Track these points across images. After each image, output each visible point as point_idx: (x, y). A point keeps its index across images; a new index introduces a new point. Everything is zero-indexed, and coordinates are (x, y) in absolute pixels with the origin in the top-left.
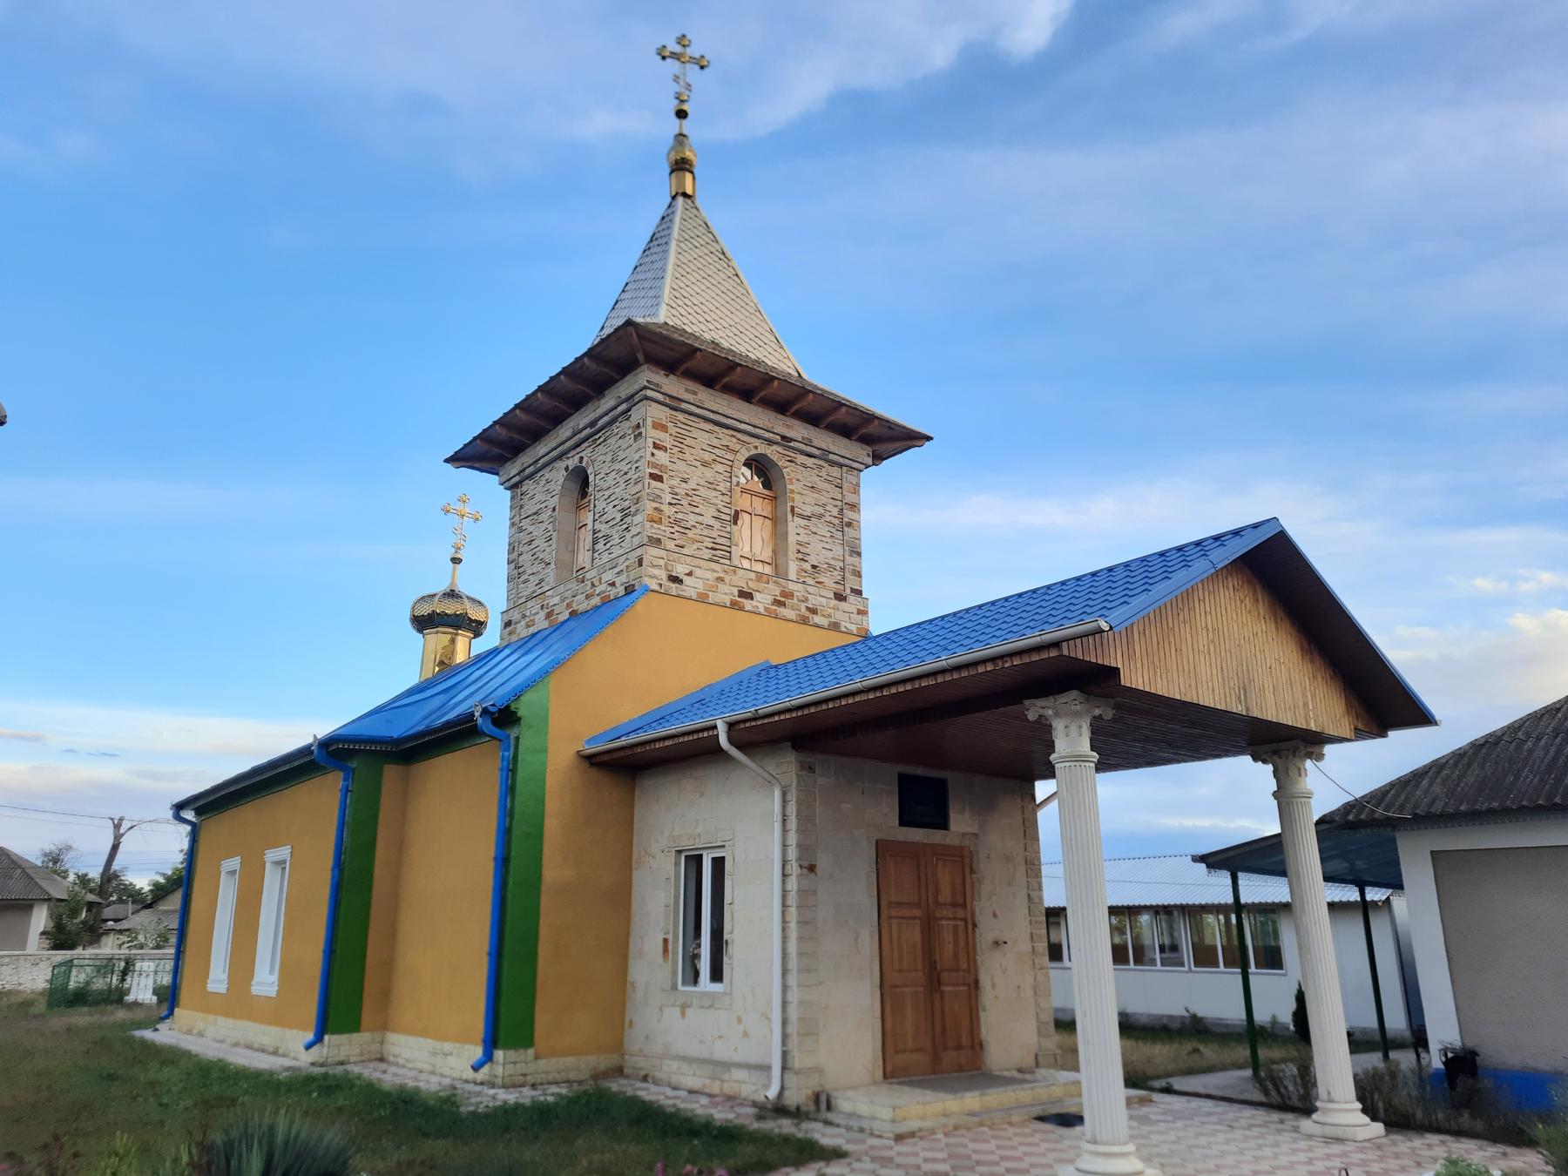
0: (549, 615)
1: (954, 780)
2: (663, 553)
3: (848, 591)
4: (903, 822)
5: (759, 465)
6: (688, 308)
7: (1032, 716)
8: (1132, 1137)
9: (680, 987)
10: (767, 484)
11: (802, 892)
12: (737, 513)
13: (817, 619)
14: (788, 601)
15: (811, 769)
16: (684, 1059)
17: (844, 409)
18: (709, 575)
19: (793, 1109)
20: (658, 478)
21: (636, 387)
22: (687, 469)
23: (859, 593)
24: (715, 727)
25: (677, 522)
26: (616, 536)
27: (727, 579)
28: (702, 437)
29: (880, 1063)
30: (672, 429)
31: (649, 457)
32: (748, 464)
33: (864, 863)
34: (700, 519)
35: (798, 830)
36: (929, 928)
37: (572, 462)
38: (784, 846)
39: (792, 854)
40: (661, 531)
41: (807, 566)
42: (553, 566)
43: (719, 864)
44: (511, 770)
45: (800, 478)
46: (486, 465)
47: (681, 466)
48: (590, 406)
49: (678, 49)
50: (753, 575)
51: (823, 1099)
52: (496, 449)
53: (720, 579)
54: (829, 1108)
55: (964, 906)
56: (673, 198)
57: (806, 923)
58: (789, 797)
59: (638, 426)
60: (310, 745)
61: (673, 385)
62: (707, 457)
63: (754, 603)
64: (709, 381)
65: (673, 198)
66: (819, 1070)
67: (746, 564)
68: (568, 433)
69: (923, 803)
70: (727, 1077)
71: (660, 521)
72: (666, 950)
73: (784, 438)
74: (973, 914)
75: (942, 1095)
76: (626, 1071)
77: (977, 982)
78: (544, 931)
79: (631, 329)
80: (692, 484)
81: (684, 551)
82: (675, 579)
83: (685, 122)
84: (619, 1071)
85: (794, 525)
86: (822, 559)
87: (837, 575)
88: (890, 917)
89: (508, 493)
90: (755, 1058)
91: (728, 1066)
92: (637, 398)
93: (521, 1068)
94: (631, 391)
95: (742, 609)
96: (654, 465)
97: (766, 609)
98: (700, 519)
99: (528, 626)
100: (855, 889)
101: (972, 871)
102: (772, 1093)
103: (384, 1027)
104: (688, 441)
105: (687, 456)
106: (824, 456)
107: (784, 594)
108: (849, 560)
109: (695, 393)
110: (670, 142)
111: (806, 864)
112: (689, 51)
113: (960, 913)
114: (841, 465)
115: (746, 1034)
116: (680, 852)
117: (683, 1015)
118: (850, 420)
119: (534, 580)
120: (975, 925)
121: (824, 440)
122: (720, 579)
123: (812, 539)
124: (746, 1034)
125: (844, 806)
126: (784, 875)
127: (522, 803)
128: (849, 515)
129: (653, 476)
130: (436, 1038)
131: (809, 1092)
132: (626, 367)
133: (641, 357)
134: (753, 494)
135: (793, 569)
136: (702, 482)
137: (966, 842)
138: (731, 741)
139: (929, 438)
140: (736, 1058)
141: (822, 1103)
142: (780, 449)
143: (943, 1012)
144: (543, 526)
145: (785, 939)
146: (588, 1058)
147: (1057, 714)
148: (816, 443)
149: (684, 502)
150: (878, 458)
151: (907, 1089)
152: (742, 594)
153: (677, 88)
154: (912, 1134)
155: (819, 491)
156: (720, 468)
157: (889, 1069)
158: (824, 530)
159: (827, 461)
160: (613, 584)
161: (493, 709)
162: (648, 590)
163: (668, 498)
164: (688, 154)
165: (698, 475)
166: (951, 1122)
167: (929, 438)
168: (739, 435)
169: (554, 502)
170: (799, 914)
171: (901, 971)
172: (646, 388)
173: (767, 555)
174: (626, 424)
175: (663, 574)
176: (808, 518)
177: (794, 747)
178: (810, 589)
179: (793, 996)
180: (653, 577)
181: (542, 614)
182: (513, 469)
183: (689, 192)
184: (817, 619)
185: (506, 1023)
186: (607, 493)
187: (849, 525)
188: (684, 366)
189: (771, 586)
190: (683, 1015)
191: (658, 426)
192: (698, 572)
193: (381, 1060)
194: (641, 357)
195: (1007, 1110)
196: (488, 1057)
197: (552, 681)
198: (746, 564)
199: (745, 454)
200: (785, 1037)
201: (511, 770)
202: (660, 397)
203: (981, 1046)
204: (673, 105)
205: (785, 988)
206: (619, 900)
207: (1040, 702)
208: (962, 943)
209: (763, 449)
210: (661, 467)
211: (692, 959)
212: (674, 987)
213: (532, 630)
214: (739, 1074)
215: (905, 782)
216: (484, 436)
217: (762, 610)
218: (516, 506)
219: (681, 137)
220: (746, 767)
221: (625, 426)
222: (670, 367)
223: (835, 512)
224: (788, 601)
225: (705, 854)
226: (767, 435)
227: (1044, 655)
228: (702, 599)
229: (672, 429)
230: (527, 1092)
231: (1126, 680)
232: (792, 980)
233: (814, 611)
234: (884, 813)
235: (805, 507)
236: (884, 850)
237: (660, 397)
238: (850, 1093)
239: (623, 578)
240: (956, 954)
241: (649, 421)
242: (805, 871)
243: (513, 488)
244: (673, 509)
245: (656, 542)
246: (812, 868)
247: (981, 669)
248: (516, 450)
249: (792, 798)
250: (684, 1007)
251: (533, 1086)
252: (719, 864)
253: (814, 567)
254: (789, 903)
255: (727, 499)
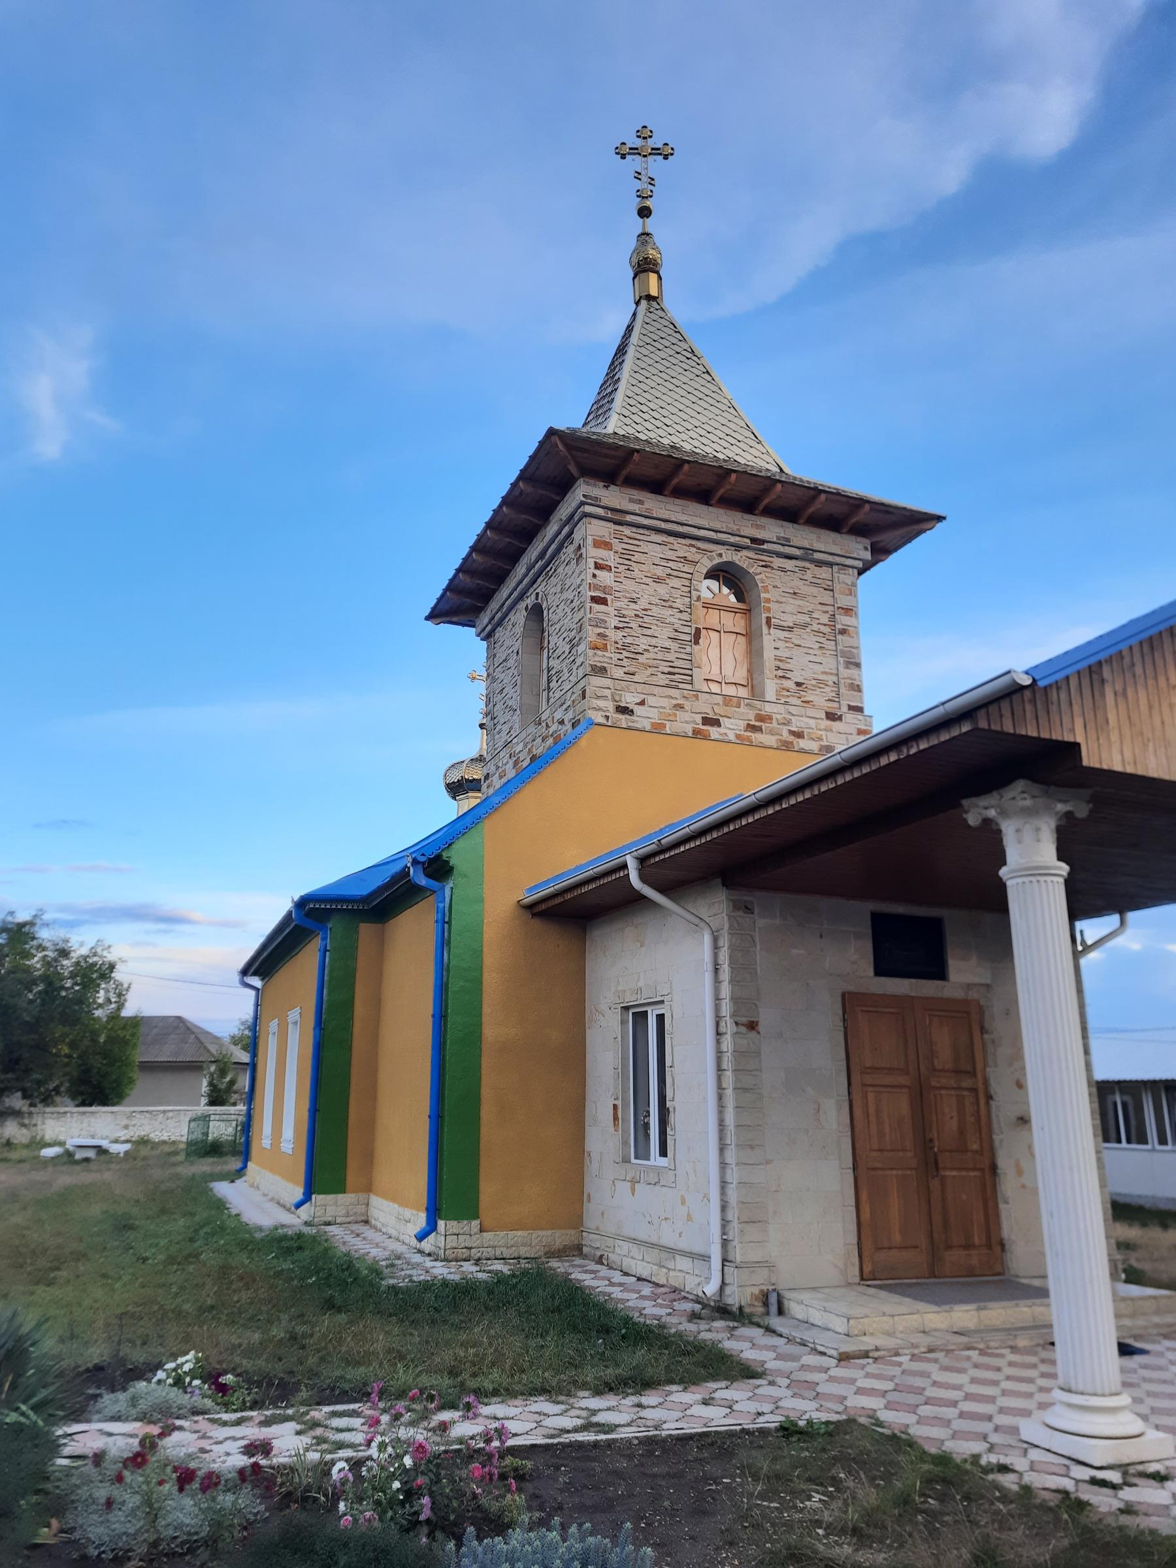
0: (516, 764)
1: (952, 918)
2: (608, 682)
3: (845, 709)
4: (879, 972)
5: (725, 574)
6: (658, 418)
7: (973, 819)
8: (1125, 1384)
9: (633, 1161)
10: (740, 597)
11: (738, 1053)
12: (698, 631)
13: (803, 744)
14: (764, 726)
15: (748, 909)
16: (634, 1241)
17: (823, 497)
18: (665, 702)
19: (735, 1309)
20: (602, 601)
21: (574, 504)
22: (638, 588)
23: (859, 710)
24: (624, 866)
25: (625, 647)
26: (565, 671)
27: (687, 705)
28: (653, 550)
29: (856, 1260)
30: (617, 546)
31: (590, 580)
32: (712, 574)
33: (825, 1023)
34: (653, 641)
35: (731, 981)
36: (921, 1096)
37: (530, 601)
38: (717, 999)
39: (726, 1009)
40: (608, 657)
41: (789, 684)
42: (518, 712)
43: (661, 1018)
44: (445, 923)
45: (776, 586)
46: (462, 618)
47: (629, 585)
48: (539, 537)
49: (638, 143)
50: (719, 699)
51: (773, 1299)
52: (469, 597)
53: (680, 707)
54: (781, 1312)
55: (973, 1074)
56: (637, 303)
57: (746, 1090)
58: (721, 943)
59: (579, 547)
60: (290, 913)
61: (615, 497)
62: (660, 572)
63: (721, 730)
64: (656, 487)
65: (637, 303)
66: (769, 1265)
67: (715, 688)
68: (524, 570)
69: (909, 947)
70: (671, 1265)
71: (605, 648)
72: (616, 1118)
73: (754, 540)
74: (986, 1082)
75: (921, 1306)
76: (585, 1250)
77: (994, 1168)
78: (486, 1093)
79: (555, 439)
80: (642, 603)
81: (636, 678)
82: (624, 710)
83: (648, 221)
84: (577, 1250)
85: (770, 641)
86: (808, 674)
87: (829, 692)
88: (864, 1085)
89: (464, 644)
90: (698, 1248)
91: (673, 1252)
92: (576, 518)
93: (464, 1241)
94: (570, 510)
95: (706, 737)
96: (596, 587)
97: (738, 736)
98: (653, 641)
99: (501, 777)
100: (815, 1046)
101: (983, 1030)
102: (711, 1289)
103: (368, 1188)
104: (637, 557)
105: (637, 573)
106: (807, 555)
107: (761, 718)
108: (844, 672)
109: (641, 502)
110: (632, 243)
111: (744, 1020)
112: (651, 143)
113: (967, 1083)
114: (830, 565)
115: (689, 1218)
116: (626, 1008)
117: (633, 1191)
118: (835, 509)
119: (506, 728)
120: (989, 1097)
121: (804, 536)
122: (680, 707)
123: (796, 652)
124: (689, 1218)
125: (795, 951)
126: (718, 1034)
127: (457, 956)
128: (843, 620)
129: (594, 599)
130: (401, 1204)
131: (756, 1290)
132: (564, 486)
133: (573, 469)
134: (720, 608)
135: (771, 689)
136: (655, 600)
137: (973, 995)
138: (643, 878)
139: (940, 519)
140: (682, 1245)
141: (773, 1303)
142: (751, 554)
143: (944, 1200)
144: (510, 672)
145: (721, 1107)
146: (541, 1233)
147: (1003, 813)
148: (795, 541)
149: (634, 625)
150: (880, 552)
151: (883, 1294)
152: (707, 721)
153: (638, 185)
154: (865, 1355)
155: (804, 597)
156: (675, 583)
157: (867, 1269)
158: (810, 640)
159: (812, 561)
160: (562, 722)
161: (422, 859)
162: (592, 723)
163: (614, 622)
164: (652, 253)
165: (648, 594)
166: (925, 1341)
167: (940, 519)
168: (699, 544)
169: (518, 645)
170: (737, 1080)
171: (881, 1150)
172: (582, 504)
173: (741, 675)
174: (572, 548)
175: (610, 706)
176: (790, 629)
177: (725, 884)
178: (792, 709)
179: (733, 1176)
180: (600, 708)
181: (511, 764)
182: (485, 618)
183: (654, 292)
184: (803, 744)
185: (450, 1192)
186: (558, 626)
187: (843, 632)
188: (624, 473)
189: (743, 709)
190: (633, 1191)
191: (600, 544)
192: (651, 700)
193: (366, 1222)
194: (573, 469)
195: (1012, 1331)
196: (431, 1227)
197: (487, 827)
198: (715, 688)
199: (706, 564)
200: (725, 1223)
201: (445, 923)
202: (600, 512)
203: (1002, 1245)
204: (635, 203)
205: (723, 1165)
206: (573, 1058)
207: (983, 801)
208: (970, 1119)
209: (728, 555)
210: (604, 589)
211: (643, 1128)
212: (626, 1160)
213: (504, 780)
214: (683, 1263)
215: (879, 922)
216: (451, 587)
217: (732, 737)
218: (491, 656)
219: (645, 236)
220: (667, 909)
221: (570, 550)
222: (609, 477)
223: (825, 619)
224: (764, 726)
225: (649, 1009)
226: (732, 539)
227: (955, 732)
228: (658, 729)
229: (617, 546)
230: (468, 1267)
231: (1090, 758)
232: (731, 1157)
233: (799, 735)
234: (851, 960)
235: (784, 617)
236: (852, 1004)
237: (600, 512)
238: (806, 1297)
239: (570, 715)
240: (962, 1132)
241: (590, 540)
242: (743, 1029)
243: (487, 638)
244: (620, 634)
245: (601, 671)
246: (752, 1026)
247: (884, 761)
248: (486, 597)
249: (724, 942)
250: (634, 1182)
251: (477, 1262)
252: (661, 1018)
253: (798, 684)
254: (725, 1066)
255: (685, 616)
